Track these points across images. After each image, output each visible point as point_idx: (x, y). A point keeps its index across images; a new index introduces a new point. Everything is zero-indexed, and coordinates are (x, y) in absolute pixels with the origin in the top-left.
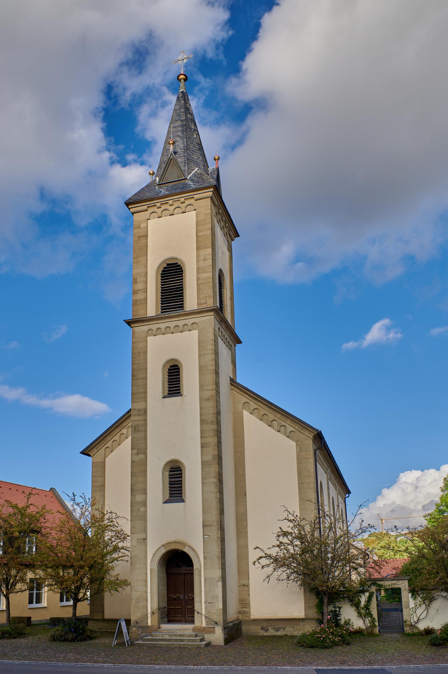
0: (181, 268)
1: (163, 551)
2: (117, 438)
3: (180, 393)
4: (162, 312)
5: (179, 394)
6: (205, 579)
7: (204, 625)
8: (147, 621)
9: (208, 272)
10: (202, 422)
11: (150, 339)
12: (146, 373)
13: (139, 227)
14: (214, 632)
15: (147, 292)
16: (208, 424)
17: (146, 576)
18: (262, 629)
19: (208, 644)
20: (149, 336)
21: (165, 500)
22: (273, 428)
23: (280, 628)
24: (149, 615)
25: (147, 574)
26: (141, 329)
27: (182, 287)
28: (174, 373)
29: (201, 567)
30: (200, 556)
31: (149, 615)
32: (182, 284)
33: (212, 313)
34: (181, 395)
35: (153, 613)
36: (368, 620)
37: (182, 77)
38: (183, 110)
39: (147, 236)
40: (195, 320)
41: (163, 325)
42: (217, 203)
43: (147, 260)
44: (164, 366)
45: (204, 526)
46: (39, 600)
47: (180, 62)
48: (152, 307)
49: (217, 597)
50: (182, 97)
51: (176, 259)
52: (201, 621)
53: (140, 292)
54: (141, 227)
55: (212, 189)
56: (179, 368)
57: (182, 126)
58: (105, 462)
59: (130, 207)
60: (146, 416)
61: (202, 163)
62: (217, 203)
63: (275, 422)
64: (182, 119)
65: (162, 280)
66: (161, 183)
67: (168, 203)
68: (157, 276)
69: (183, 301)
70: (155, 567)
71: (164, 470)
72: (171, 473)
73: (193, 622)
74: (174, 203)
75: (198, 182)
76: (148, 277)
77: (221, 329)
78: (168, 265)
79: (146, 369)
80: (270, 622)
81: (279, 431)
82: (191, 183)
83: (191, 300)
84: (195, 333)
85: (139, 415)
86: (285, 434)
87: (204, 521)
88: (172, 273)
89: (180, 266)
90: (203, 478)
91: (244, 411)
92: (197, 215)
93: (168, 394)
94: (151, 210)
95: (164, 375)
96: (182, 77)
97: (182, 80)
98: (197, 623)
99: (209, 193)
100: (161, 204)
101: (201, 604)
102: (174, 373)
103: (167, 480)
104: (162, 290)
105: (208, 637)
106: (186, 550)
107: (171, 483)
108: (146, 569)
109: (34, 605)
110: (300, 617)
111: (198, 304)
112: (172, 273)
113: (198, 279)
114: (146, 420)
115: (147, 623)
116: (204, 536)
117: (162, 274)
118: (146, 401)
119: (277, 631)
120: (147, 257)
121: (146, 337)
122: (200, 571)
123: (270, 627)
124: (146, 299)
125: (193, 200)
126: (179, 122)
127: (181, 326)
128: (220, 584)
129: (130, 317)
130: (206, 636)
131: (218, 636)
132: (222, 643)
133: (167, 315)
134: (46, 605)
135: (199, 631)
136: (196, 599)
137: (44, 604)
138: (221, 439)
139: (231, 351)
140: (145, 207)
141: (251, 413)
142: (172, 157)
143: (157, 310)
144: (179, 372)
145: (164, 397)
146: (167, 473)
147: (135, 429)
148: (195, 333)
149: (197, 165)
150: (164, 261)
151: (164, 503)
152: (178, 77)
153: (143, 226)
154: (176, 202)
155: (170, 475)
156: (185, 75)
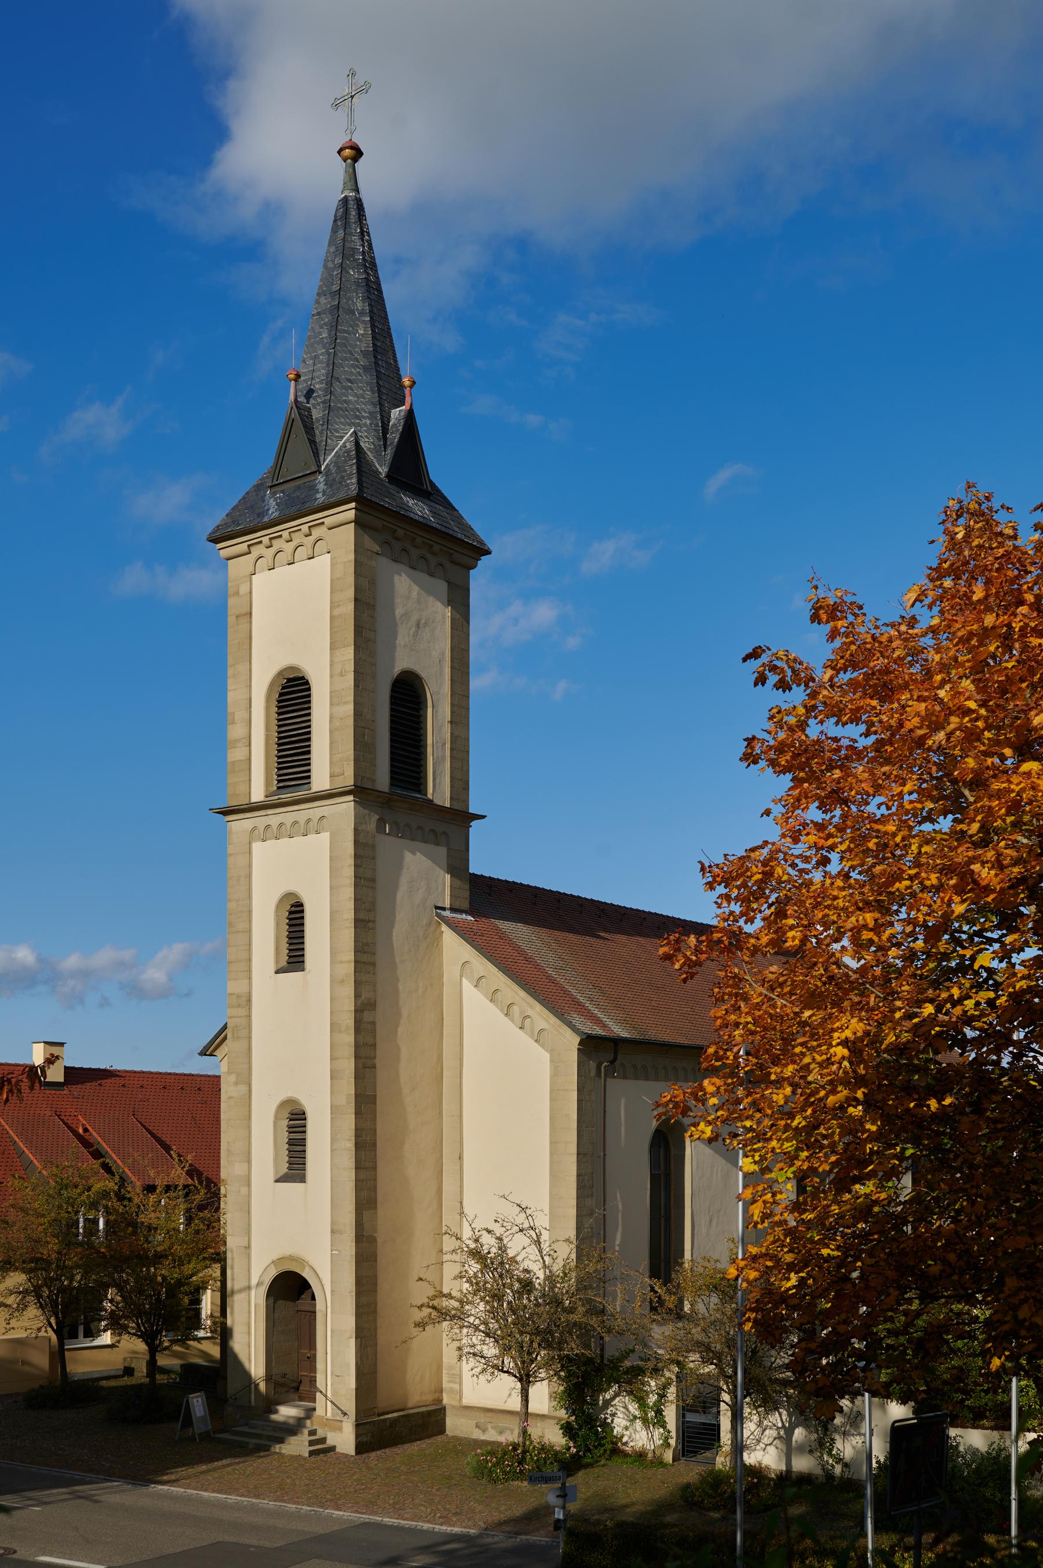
4: (279, 788)
6: (332, 1331)
9: (345, 703)
10: (334, 1027)
11: (257, 846)
12: (250, 921)
13: (237, 593)
14: (340, 1429)
16: (340, 1032)
17: (249, 1317)
18: (477, 1426)
20: (256, 841)
21: (278, 1176)
23: (507, 1428)
25: (249, 1312)
26: (240, 825)
33: (351, 798)
36: (658, 1432)
39: (251, 614)
41: (274, 818)
43: (250, 670)
44: (278, 907)
45: (332, 1232)
49: (348, 1364)
53: (239, 745)
54: (241, 593)
55: (353, 505)
60: (250, 1009)
65: (279, 714)
67: (323, 523)
71: (277, 1118)
72: (292, 1122)
74: (274, 542)
78: (289, 680)
79: (250, 912)
80: (490, 1414)
84: (325, 836)
85: (239, 1006)
87: (333, 1223)
90: (333, 1140)
91: (464, 980)
92: (333, 565)
94: (256, 551)
95: (277, 924)
100: (271, 539)
104: (279, 738)
106: (306, 1274)
107: (291, 1143)
110: (541, 1413)
114: (249, 1016)
115: (250, 1401)
117: (279, 702)
118: (250, 979)
119: (501, 1433)
120: (250, 663)
121: (250, 843)
123: (489, 1426)
125: (324, 528)
127: (302, 822)
132: (353, 1453)
133: (286, 796)
140: (244, 547)
143: (268, 784)
148: (325, 836)
150: (280, 674)
151: (277, 1181)
153: (244, 589)
155: (289, 1127)
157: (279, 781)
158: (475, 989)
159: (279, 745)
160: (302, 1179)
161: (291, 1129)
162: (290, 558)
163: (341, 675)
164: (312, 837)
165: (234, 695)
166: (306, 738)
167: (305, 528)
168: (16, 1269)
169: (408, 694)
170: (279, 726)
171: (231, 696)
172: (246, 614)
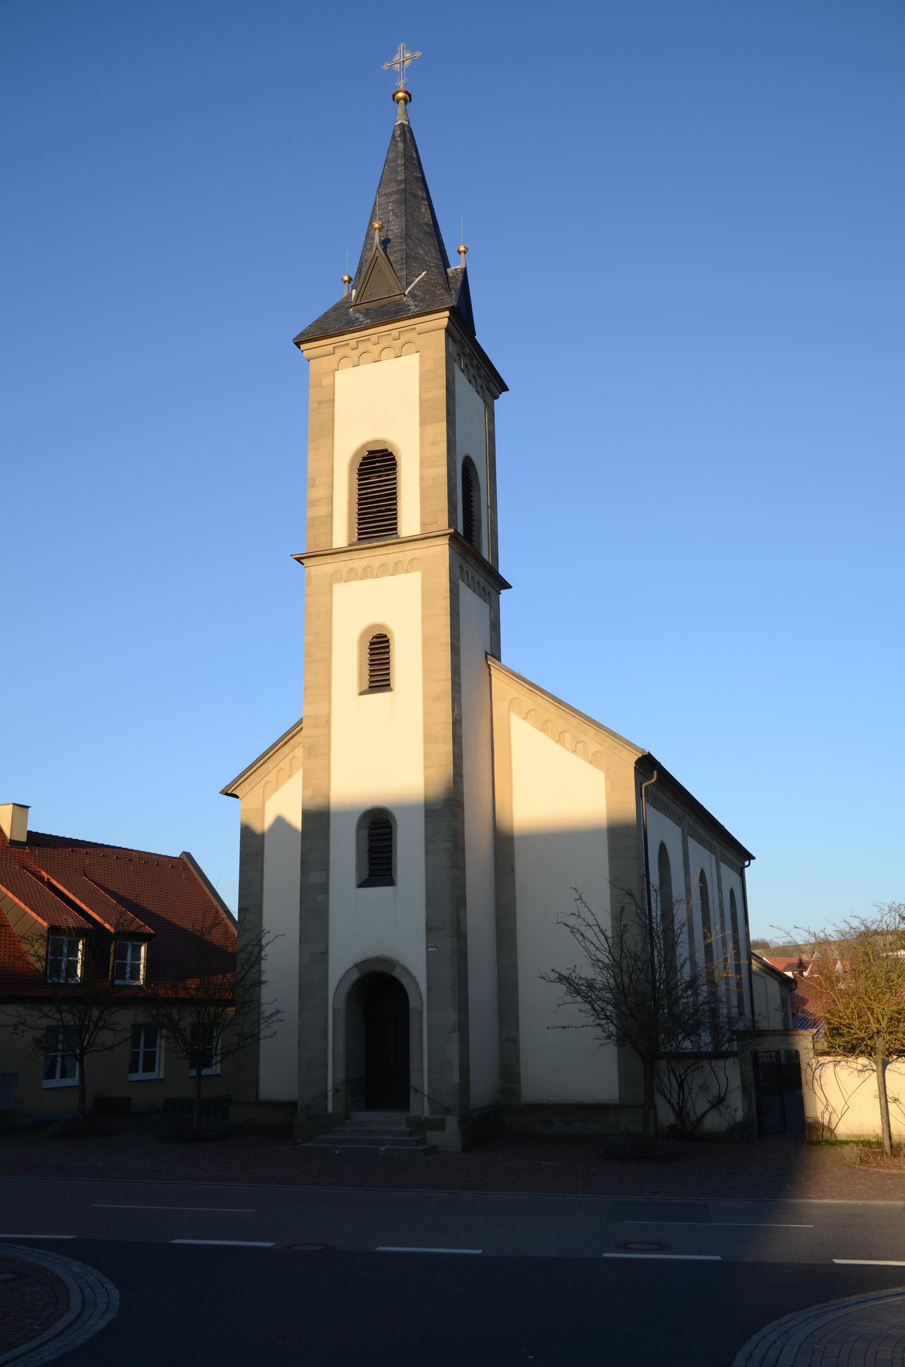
0: (394, 459)
1: (356, 975)
2: (272, 776)
3: (389, 685)
4: (359, 539)
5: (387, 688)
7: (427, 1113)
8: (326, 1105)
13: (320, 385)
15: (332, 503)
19: (434, 1149)
20: (337, 582)
22: (564, 746)
24: (330, 1094)
26: (318, 569)
27: (395, 493)
28: (379, 648)
29: (422, 1004)
30: (420, 984)
31: (330, 1094)
32: (395, 488)
34: (391, 690)
35: (336, 1090)
37: (401, 95)
38: (401, 162)
39: (334, 401)
40: (416, 553)
42: (458, 337)
46: (149, 1066)
47: (398, 65)
48: (342, 530)
50: (399, 136)
51: (384, 442)
52: (421, 1107)
55: (447, 313)
56: (388, 641)
57: (398, 192)
58: (263, 808)
59: (302, 346)
61: (435, 261)
62: (458, 337)
63: (566, 734)
64: (399, 178)
65: (359, 480)
66: (358, 302)
68: (350, 474)
69: (396, 519)
70: (342, 1005)
72: (372, 831)
73: (403, 1104)
75: (423, 300)
76: (335, 475)
77: (467, 567)
78: (370, 452)
81: (574, 752)
82: (411, 303)
83: (410, 515)
86: (585, 756)
88: (377, 466)
89: (391, 454)
91: (512, 714)
93: (370, 687)
94: (340, 353)
96: (401, 95)
97: (402, 102)
98: (414, 1111)
99: (442, 319)
101: (422, 1077)
102: (379, 648)
103: (365, 844)
104: (359, 499)
105: (433, 1137)
106: (397, 974)
107: (371, 851)
108: (326, 1008)
109: (141, 1075)
111: (423, 525)
112: (377, 466)
113: (422, 479)
115: (326, 1109)
116: (427, 948)
117: (359, 470)
121: (331, 585)
122: (421, 1013)
124: (331, 515)
126: (394, 184)
128: (455, 1037)
129: (301, 550)
130: (429, 1134)
131: (450, 1135)
134: (162, 1076)
135: (419, 1126)
136: (413, 1065)
137: (159, 1072)
138: (462, 769)
139: (490, 604)
141: (524, 719)
142: (377, 254)
143: (350, 535)
144: (388, 647)
145: (361, 694)
146: (365, 832)
147: (311, 752)
149: (424, 266)
150: (364, 446)
152: (394, 96)
153: (326, 382)
154: (385, 338)
155: (370, 835)
156: (406, 92)
157: (359, 534)
158: (524, 722)
159: (359, 505)
160: (391, 882)
161: (372, 838)
162: (356, 362)
163: (433, 444)
164: (401, 578)
165: (314, 464)
166: (392, 497)
167: (353, 343)
168: (834, 942)
169: (468, 466)
170: (359, 490)
171: (311, 465)
172: (329, 401)
